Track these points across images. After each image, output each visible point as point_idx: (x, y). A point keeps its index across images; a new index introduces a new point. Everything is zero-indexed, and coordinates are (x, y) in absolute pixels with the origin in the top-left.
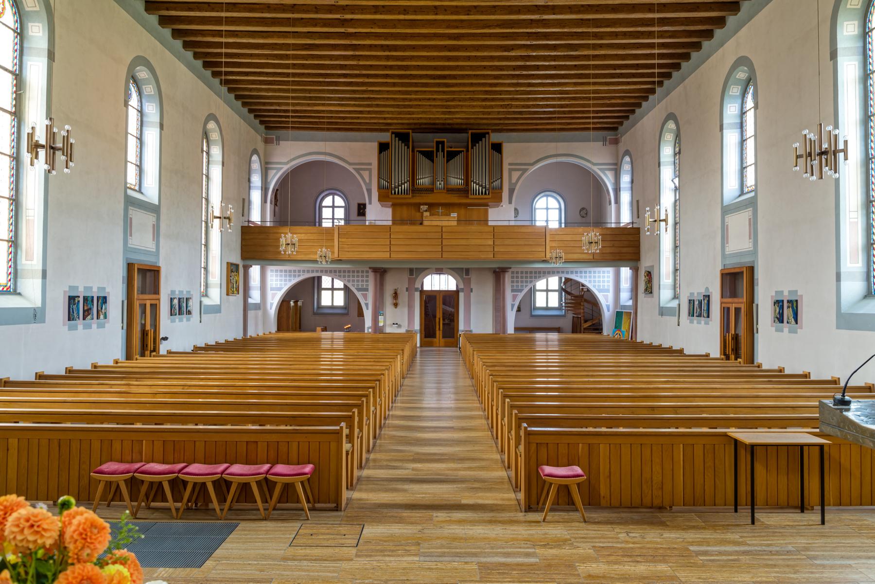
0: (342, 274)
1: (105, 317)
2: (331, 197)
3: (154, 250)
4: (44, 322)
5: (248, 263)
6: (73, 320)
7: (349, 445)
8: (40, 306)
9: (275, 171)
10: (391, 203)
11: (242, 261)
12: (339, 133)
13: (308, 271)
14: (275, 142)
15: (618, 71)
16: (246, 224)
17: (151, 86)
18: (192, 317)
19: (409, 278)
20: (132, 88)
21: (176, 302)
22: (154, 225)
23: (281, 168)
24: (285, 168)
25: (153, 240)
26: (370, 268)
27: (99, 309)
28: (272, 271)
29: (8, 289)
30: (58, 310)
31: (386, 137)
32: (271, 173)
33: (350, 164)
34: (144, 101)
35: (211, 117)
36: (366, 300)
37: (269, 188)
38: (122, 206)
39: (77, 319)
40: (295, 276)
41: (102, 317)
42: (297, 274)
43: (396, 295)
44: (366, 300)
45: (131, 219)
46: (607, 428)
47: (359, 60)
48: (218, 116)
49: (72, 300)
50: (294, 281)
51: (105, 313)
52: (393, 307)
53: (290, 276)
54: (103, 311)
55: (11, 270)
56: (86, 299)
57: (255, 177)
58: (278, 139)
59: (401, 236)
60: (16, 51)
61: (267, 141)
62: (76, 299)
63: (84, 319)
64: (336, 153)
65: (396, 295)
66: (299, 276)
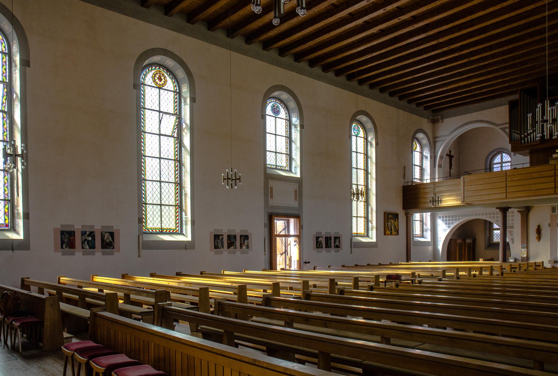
0: (492, 216)
1: (248, 247)
2: (499, 156)
3: (297, 206)
4: (194, 249)
5: (410, 211)
6: (218, 248)
7: (144, 306)
8: (191, 240)
9: (440, 143)
10: (528, 151)
11: (404, 211)
12: (488, 103)
13: (466, 216)
14: (440, 121)
15: (360, 21)
16: (406, 184)
17: (292, 102)
18: (342, 249)
19: (551, 216)
20: (280, 107)
21: (323, 240)
22: (296, 191)
23: (445, 140)
24: (448, 139)
25: (296, 199)
26: (497, 208)
27: (242, 242)
28: (440, 217)
29: (177, 231)
30: (208, 242)
31: (516, 97)
32: (438, 144)
33: (497, 125)
34: (290, 112)
35: (421, 131)
36: (512, 236)
37: (437, 156)
38: (262, 180)
39: (221, 248)
40: (456, 220)
41: (244, 247)
42: (457, 218)
43: (539, 231)
44: (512, 236)
45: (272, 189)
46: (392, 321)
47: (438, 39)
48: (368, 112)
49: (217, 237)
50: (456, 224)
51: (248, 245)
52: (536, 240)
53: (452, 220)
54: (245, 244)
55: (421, 230)
56: (229, 237)
57: (426, 150)
58: (442, 118)
59: (516, 179)
60: (176, 102)
61: (434, 122)
62: (220, 237)
63: (228, 248)
64: (474, 120)
65: (539, 231)
66: (459, 219)
